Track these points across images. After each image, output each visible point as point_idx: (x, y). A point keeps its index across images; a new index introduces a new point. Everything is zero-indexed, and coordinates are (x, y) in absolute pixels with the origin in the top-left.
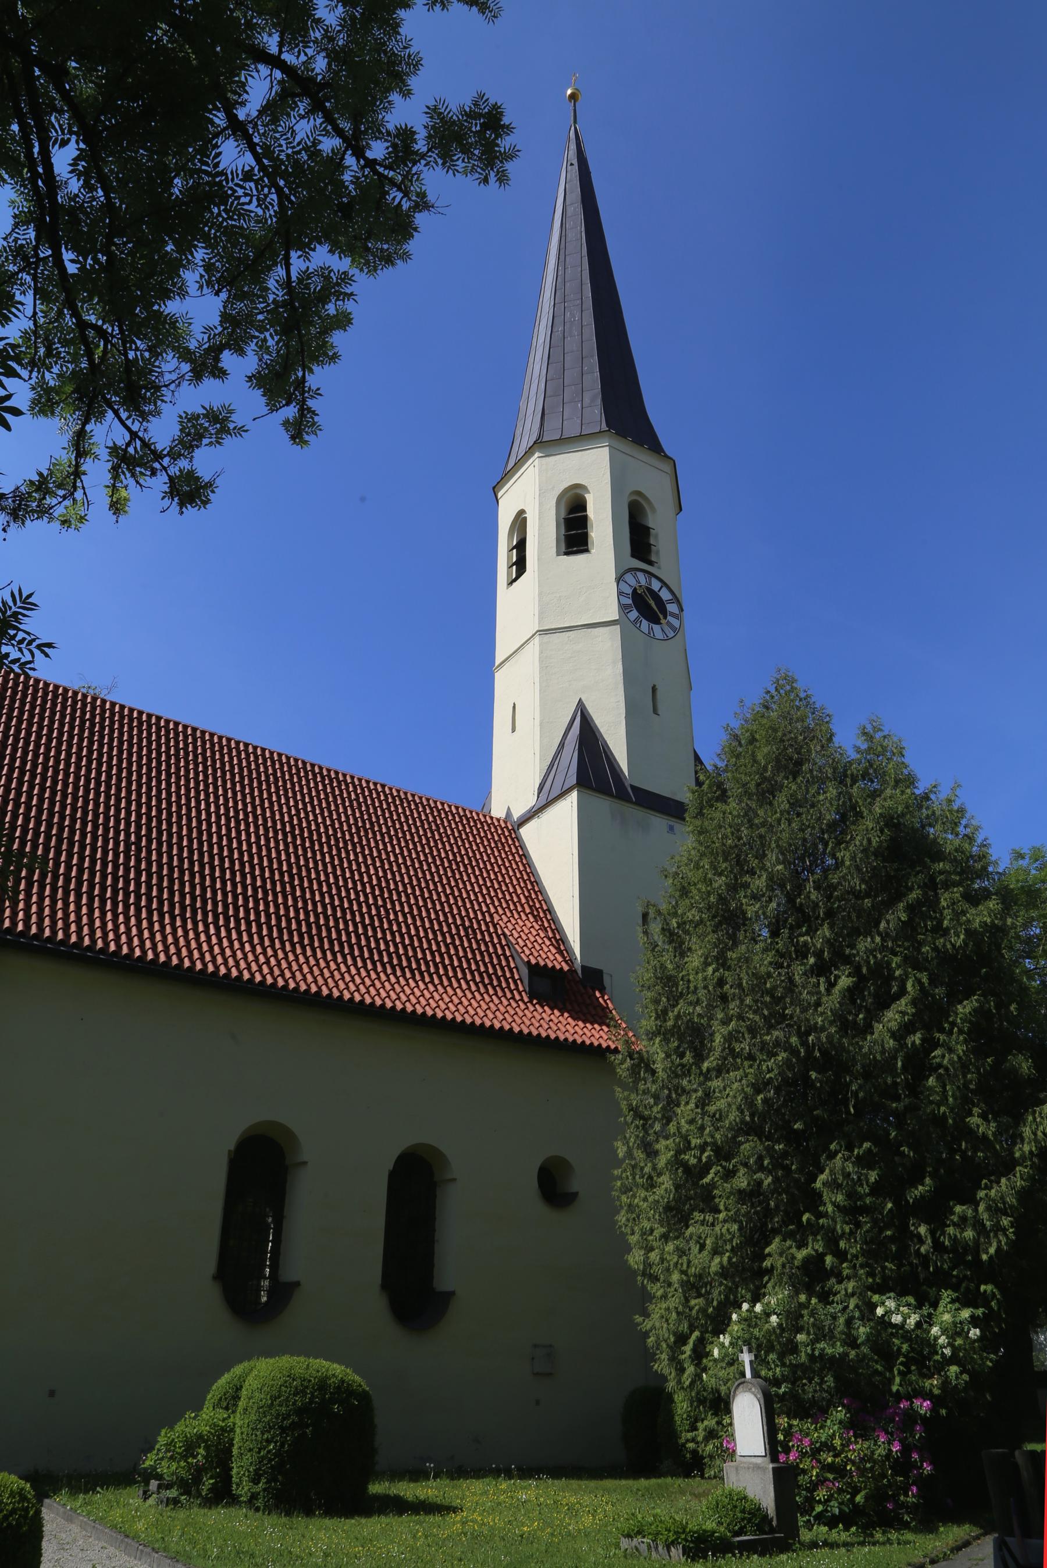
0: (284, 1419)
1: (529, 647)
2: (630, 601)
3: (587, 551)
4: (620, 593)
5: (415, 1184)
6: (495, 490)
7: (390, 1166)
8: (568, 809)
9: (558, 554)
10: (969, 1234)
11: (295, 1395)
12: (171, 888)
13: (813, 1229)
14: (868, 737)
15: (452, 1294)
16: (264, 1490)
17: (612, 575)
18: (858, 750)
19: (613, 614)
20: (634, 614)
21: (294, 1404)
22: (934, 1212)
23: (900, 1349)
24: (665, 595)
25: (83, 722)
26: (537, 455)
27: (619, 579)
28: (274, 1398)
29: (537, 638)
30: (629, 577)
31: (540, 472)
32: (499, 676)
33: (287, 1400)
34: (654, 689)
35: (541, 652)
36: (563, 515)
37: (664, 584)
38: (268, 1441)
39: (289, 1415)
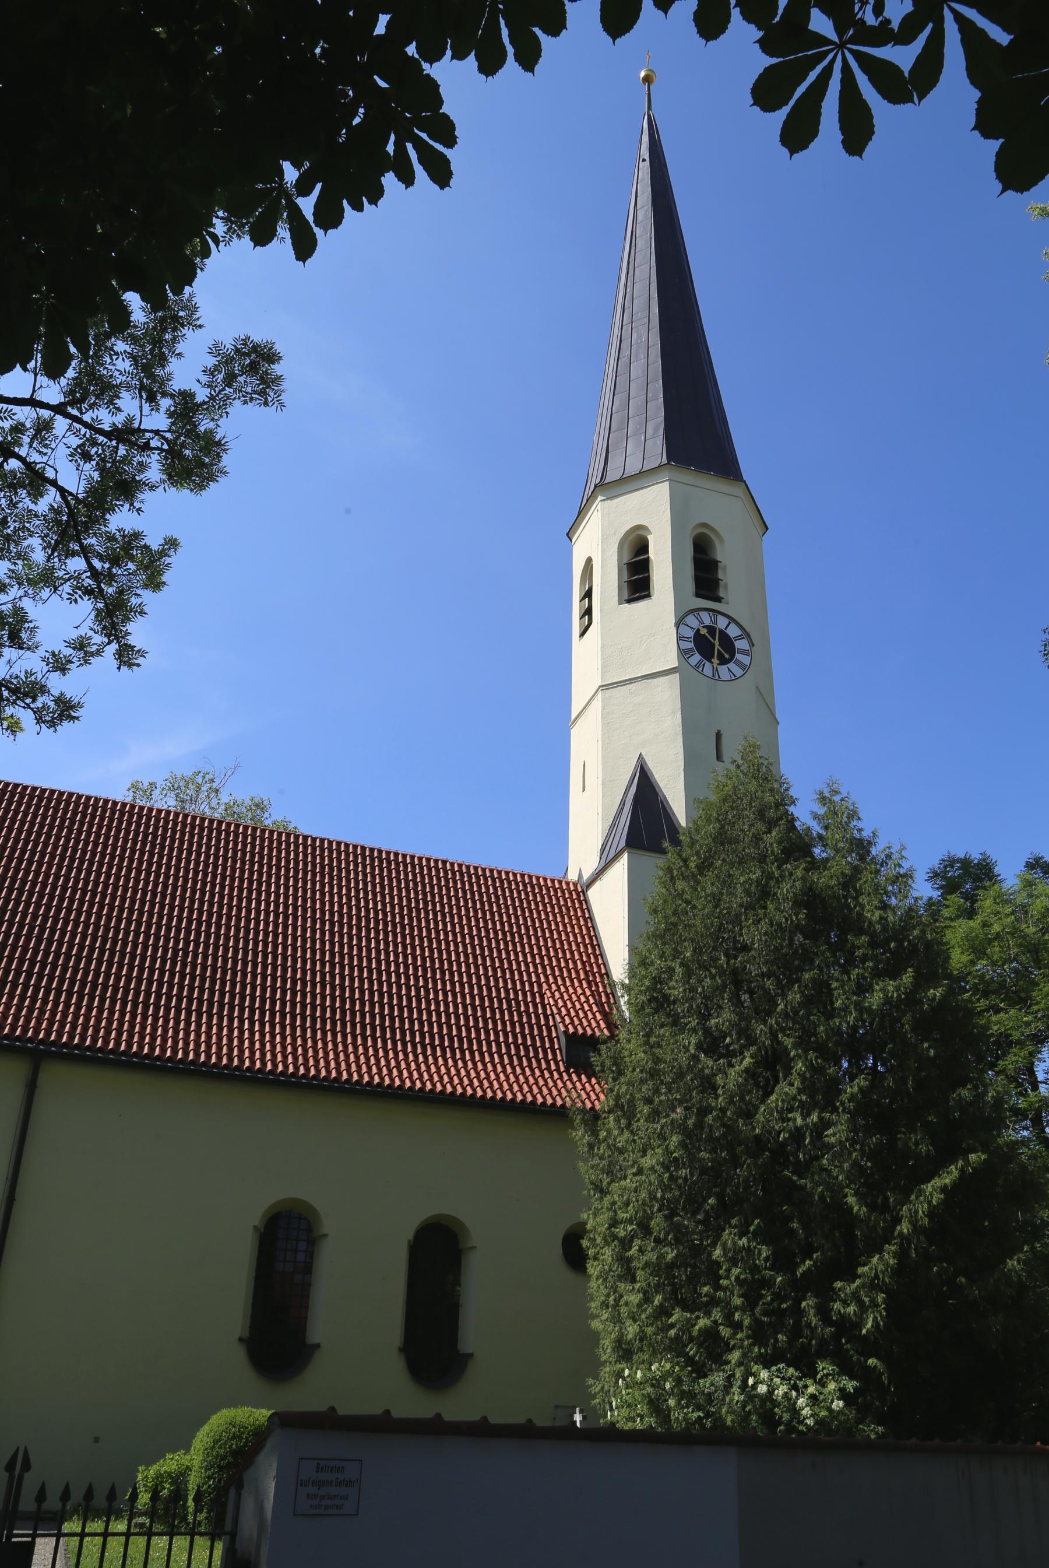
0: (222, 1459)
1: (594, 702)
2: (692, 645)
3: (649, 596)
4: (680, 638)
5: (437, 1253)
6: (569, 536)
7: (410, 1236)
8: (620, 869)
9: (620, 603)
10: (851, 1309)
11: (232, 1439)
12: (386, 940)
13: (713, 1302)
14: (823, 799)
15: (471, 1355)
16: (206, 1518)
17: (672, 620)
18: (815, 816)
19: (671, 659)
20: (697, 657)
21: (231, 1447)
22: (820, 1284)
23: (781, 1417)
24: (733, 631)
25: (146, 835)
26: (600, 498)
27: (678, 625)
28: (215, 1442)
29: (600, 693)
30: (691, 620)
31: (602, 516)
32: (574, 732)
33: (225, 1444)
34: (718, 735)
35: (603, 708)
36: (626, 559)
37: (732, 619)
38: (209, 1478)
39: (226, 1456)
